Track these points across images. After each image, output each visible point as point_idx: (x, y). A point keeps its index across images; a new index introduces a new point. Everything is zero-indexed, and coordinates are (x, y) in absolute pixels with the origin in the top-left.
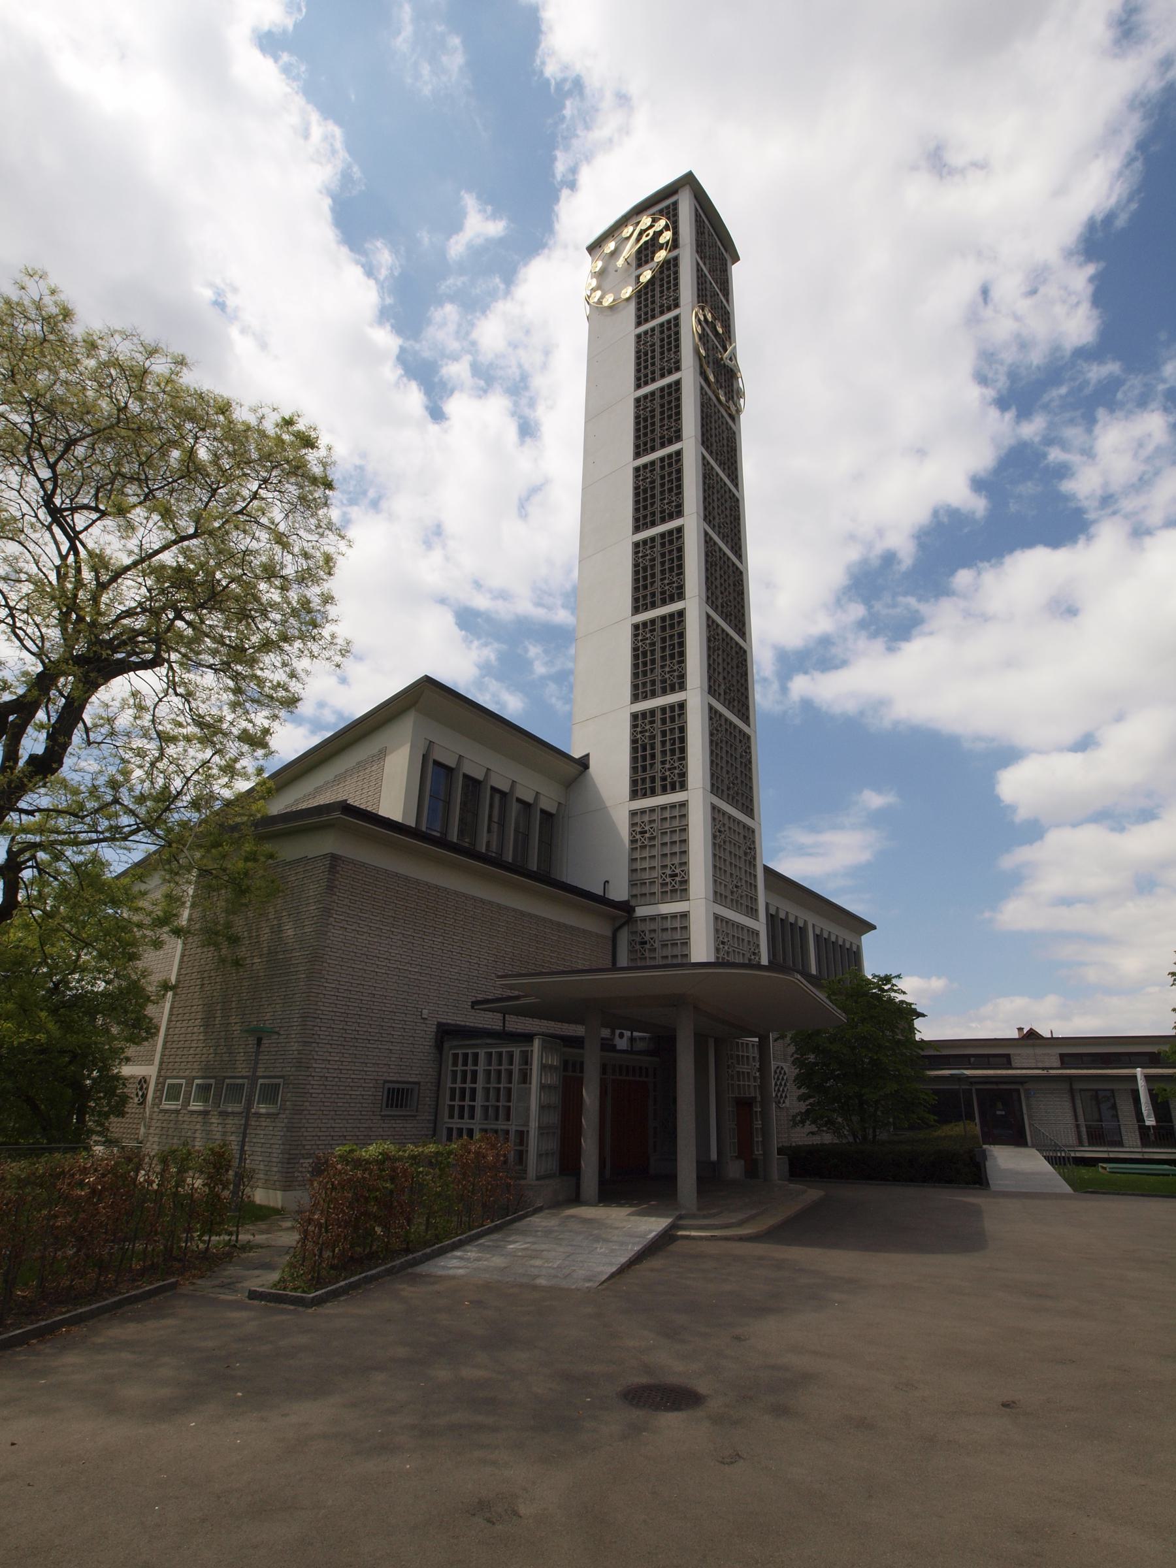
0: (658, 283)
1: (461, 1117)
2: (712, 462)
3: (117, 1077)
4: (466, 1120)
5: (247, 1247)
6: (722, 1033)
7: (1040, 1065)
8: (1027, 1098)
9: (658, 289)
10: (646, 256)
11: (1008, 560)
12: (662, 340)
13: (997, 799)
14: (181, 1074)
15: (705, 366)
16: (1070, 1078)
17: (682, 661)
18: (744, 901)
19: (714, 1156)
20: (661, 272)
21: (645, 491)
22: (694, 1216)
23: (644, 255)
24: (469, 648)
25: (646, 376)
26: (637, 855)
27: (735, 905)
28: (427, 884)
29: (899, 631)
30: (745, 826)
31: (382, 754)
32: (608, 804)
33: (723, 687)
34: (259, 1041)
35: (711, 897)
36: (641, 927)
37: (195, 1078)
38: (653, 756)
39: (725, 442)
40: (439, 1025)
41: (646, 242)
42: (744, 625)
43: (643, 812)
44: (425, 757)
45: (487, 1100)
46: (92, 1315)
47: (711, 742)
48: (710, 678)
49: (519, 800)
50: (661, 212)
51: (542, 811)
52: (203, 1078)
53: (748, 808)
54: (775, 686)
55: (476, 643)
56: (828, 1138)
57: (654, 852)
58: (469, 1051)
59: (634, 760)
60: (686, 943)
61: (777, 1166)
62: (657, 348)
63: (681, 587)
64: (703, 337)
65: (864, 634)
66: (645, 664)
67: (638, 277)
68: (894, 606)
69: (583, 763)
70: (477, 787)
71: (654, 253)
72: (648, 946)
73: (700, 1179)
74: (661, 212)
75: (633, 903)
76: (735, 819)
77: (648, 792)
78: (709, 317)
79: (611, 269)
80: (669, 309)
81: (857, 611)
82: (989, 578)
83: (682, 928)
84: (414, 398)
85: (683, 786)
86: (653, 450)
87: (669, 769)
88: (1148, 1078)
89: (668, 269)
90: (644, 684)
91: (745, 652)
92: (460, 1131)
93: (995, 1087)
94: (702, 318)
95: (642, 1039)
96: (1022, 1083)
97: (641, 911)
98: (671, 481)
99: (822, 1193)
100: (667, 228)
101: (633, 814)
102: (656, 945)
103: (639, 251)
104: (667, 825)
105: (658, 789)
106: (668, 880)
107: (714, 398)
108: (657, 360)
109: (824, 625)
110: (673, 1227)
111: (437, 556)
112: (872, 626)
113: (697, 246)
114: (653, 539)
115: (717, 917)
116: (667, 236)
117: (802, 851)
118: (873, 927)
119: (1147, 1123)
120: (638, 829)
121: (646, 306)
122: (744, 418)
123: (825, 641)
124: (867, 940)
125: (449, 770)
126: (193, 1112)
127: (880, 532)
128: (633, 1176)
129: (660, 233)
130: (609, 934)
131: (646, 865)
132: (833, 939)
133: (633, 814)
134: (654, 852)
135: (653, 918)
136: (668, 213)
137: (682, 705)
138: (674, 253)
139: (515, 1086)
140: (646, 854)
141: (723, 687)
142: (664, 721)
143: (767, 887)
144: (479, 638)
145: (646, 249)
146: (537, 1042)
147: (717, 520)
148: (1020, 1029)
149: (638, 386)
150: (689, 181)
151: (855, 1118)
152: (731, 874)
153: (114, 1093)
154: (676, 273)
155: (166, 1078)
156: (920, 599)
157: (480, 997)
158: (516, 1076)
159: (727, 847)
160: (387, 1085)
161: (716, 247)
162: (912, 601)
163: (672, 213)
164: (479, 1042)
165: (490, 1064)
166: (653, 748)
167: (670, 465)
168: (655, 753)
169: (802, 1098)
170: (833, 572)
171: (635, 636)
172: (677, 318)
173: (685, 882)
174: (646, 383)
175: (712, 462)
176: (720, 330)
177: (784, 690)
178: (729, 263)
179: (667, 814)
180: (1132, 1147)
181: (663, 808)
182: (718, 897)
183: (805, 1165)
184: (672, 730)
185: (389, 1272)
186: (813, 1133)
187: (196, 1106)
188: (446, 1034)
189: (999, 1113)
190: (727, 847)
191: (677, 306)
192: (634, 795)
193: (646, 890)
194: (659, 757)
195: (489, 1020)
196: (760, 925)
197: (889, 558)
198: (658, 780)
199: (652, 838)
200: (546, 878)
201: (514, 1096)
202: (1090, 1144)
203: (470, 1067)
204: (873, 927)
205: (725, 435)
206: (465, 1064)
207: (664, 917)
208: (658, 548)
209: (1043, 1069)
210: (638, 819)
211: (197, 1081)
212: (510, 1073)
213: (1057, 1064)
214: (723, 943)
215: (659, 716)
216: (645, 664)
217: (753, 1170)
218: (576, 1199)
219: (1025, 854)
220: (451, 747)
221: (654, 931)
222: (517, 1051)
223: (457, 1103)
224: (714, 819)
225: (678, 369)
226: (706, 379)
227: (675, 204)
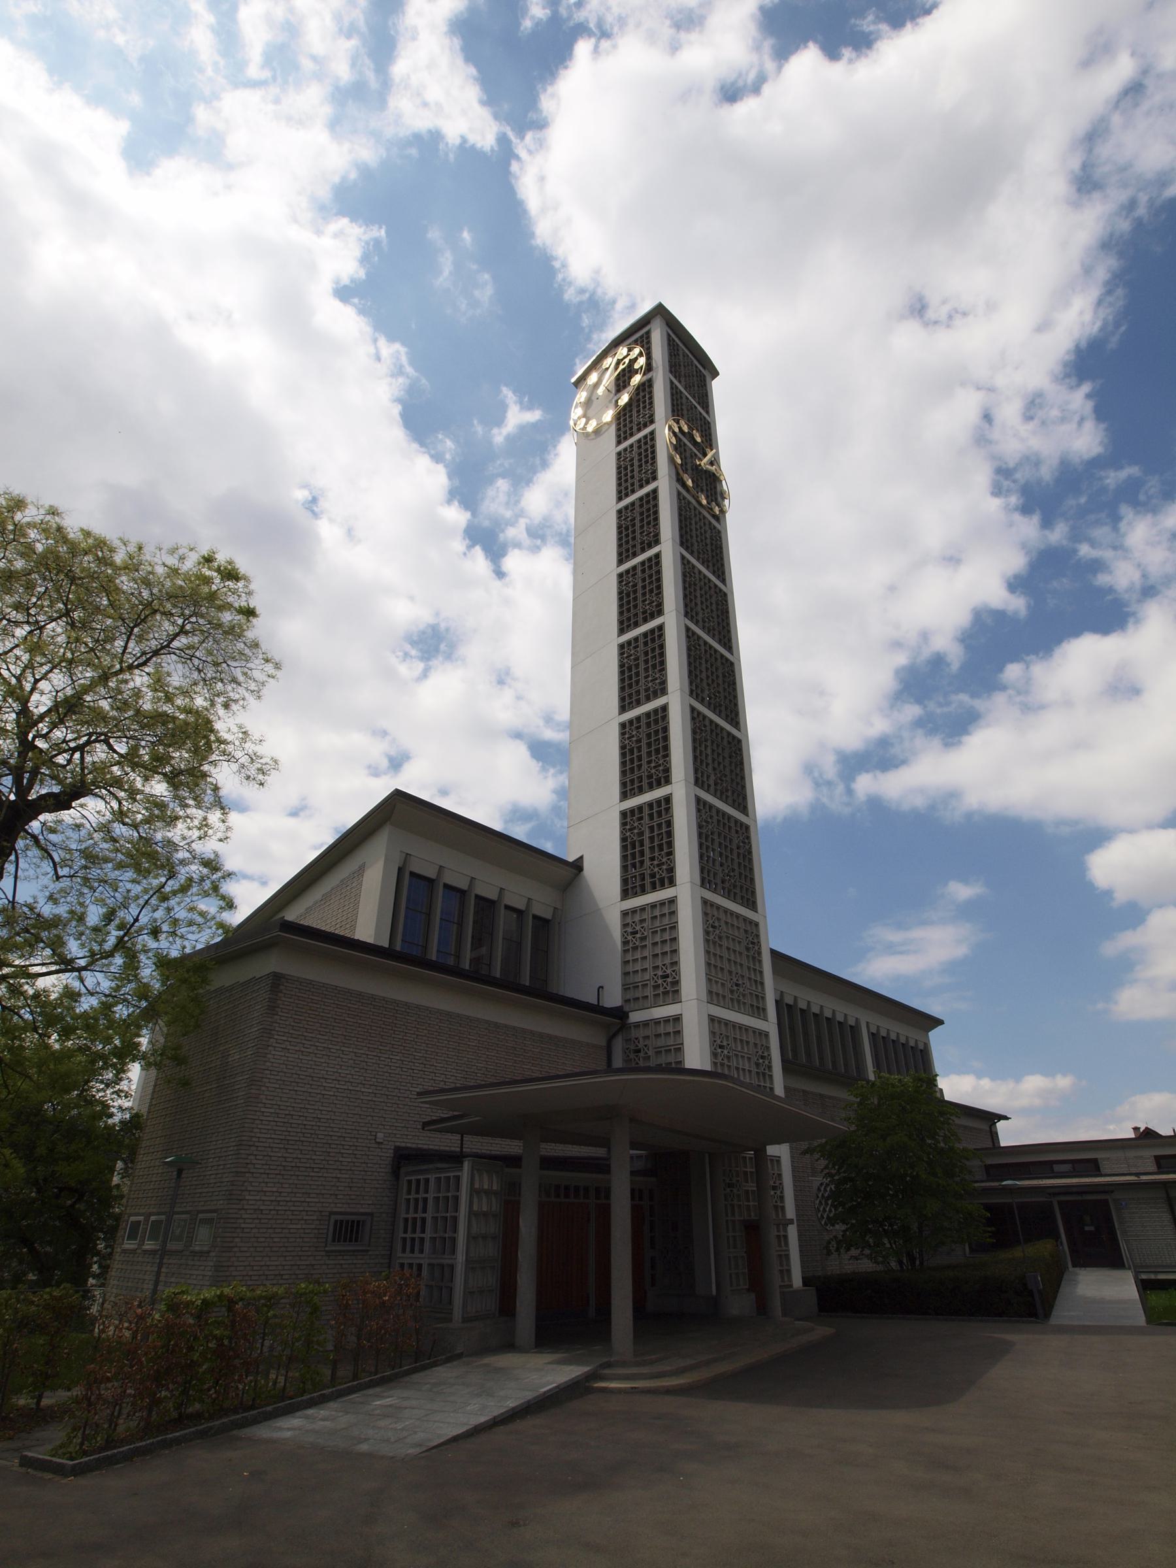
0: (635, 404)
2: (694, 561)
4: (417, 1254)
7: (1134, 1170)
11: (1058, 652)
12: (640, 454)
15: (681, 472)
17: (667, 755)
18: (748, 1000)
20: (638, 394)
22: (624, 1364)
23: (621, 382)
24: (546, 778)
25: (626, 488)
27: (736, 1003)
28: (384, 999)
29: (955, 728)
30: (745, 919)
31: (361, 869)
33: (713, 777)
34: (180, 1172)
36: (634, 1033)
37: (151, 1214)
38: (642, 853)
41: (623, 370)
43: (634, 911)
47: (700, 835)
48: (696, 771)
50: (636, 342)
51: (535, 917)
55: (552, 771)
57: (646, 953)
60: (679, 1049)
62: (636, 463)
63: (664, 683)
64: (679, 447)
65: (920, 732)
67: (617, 402)
68: (948, 704)
69: (577, 866)
72: (642, 1054)
75: (626, 1009)
76: (732, 913)
78: (686, 429)
79: (594, 398)
80: (645, 426)
81: (912, 711)
82: (1038, 669)
85: (672, 882)
86: (635, 555)
89: (644, 390)
90: (632, 781)
93: (1079, 1198)
94: (677, 430)
97: (635, 1017)
99: (829, 1331)
100: (641, 354)
101: (625, 914)
102: (650, 1053)
103: (618, 378)
104: (657, 923)
105: (648, 887)
106: (660, 981)
107: (693, 501)
109: (880, 726)
111: (508, 695)
112: (928, 725)
113: (671, 367)
115: (712, 1019)
116: (642, 361)
118: (941, 1022)
120: (629, 930)
122: (730, 518)
123: (883, 742)
124: (935, 1036)
126: (145, 1252)
127: (925, 636)
128: (570, 1319)
129: (636, 359)
130: (604, 1043)
131: (638, 967)
132: (903, 1040)
133: (625, 914)
134: (646, 953)
135: (646, 1024)
137: (668, 799)
140: (638, 955)
141: (713, 777)
142: (651, 816)
144: (554, 766)
145: (624, 375)
146: (466, 1165)
147: (701, 615)
148: (1136, 1129)
149: (620, 499)
150: (660, 311)
154: (651, 393)
156: (974, 695)
157: (428, 1119)
159: (725, 943)
161: (691, 368)
162: (964, 697)
163: (645, 342)
164: (431, 1166)
166: (642, 845)
168: (644, 848)
170: (882, 676)
172: (652, 433)
173: (677, 983)
174: (627, 495)
175: (694, 561)
176: (699, 440)
177: (850, 792)
178: (708, 378)
179: (657, 912)
181: (653, 906)
182: (713, 996)
184: (660, 825)
185: (203, 1434)
187: (149, 1245)
188: (404, 1158)
189: (1087, 1228)
191: (652, 422)
192: (626, 894)
193: (639, 994)
194: (647, 854)
195: (448, 1142)
196: (770, 1025)
198: (647, 877)
199: (643, 939)
203: (422, 1195)
204: (941, 1022)
207: (657, 1022)
208: (641, 647)
209: (1137, 1175)
210: (629, 920)
211: (153, 1218)
213: (1154, 1168)
214: (721, 1047)
215: (646, 811)
218: (509, 1346)
220: (430, 859)
221: (648, 1037)
224: (705, 914)
226: (684, 485)
227: (648, 333)
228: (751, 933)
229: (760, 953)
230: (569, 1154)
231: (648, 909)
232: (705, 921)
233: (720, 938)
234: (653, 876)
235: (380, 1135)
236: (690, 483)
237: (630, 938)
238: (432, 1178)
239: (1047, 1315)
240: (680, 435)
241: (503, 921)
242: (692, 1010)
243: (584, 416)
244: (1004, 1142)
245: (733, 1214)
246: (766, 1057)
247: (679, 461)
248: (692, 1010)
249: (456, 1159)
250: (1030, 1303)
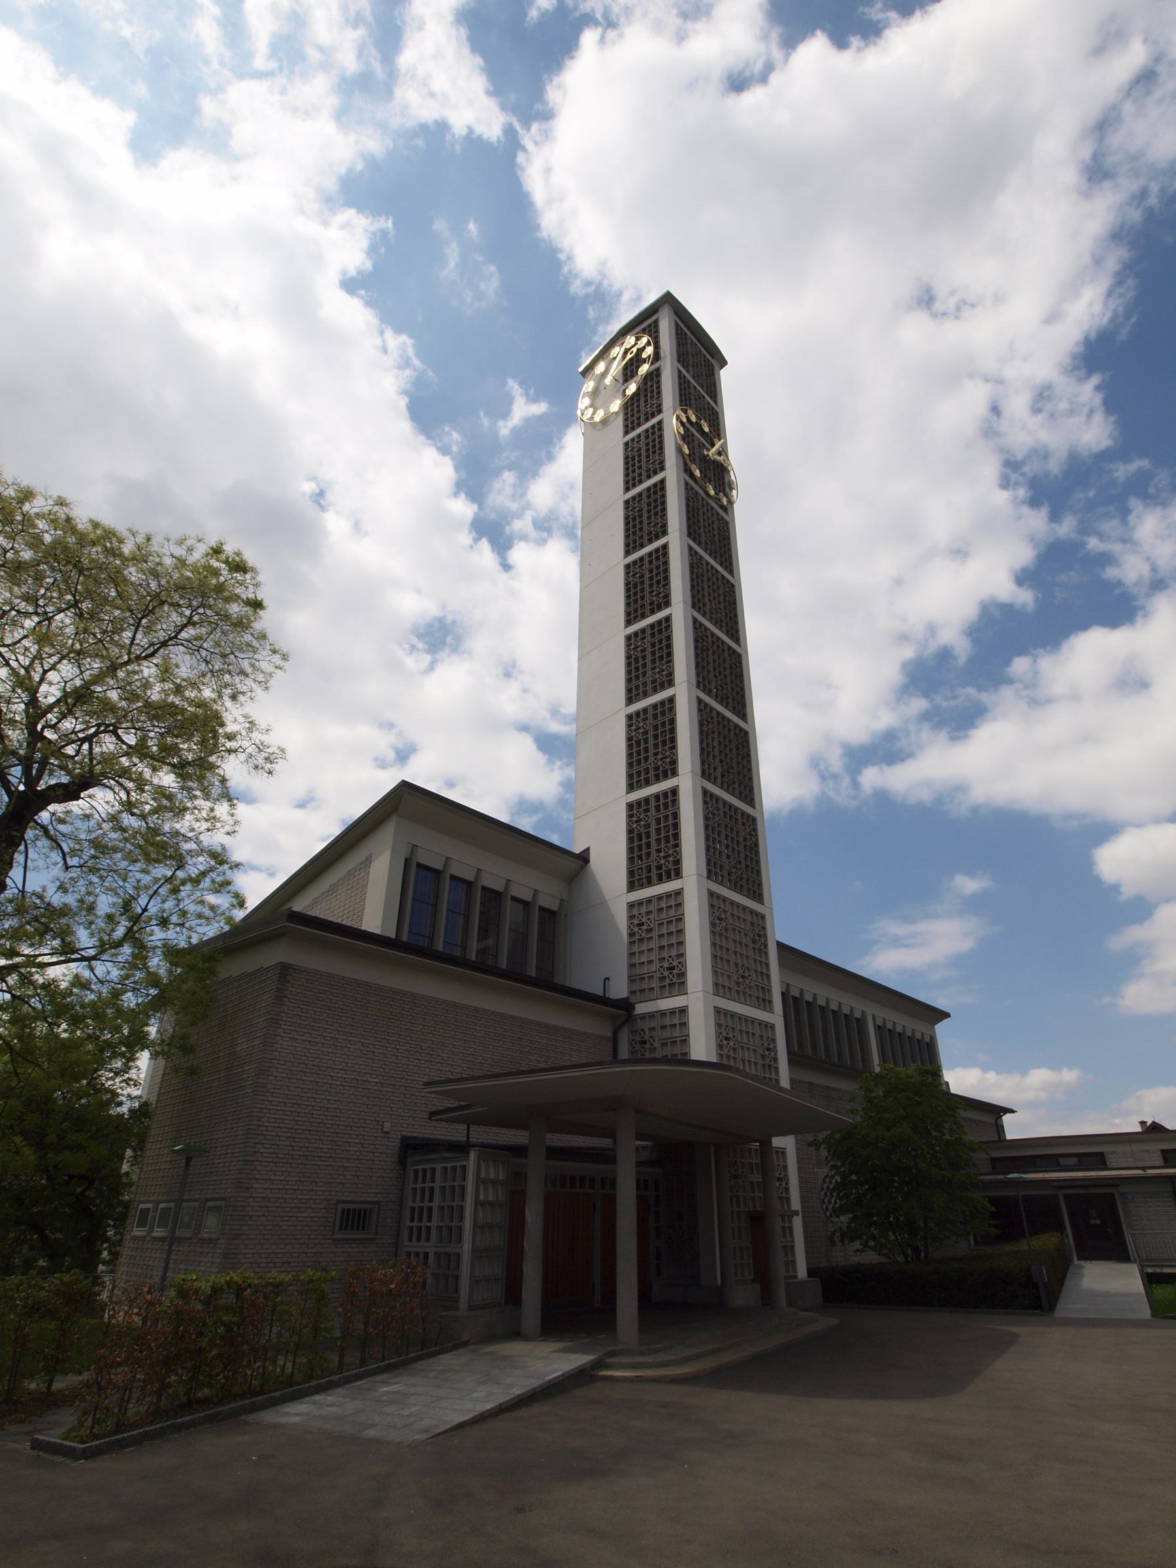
0: (642, 394)
2: (701, 552)
9: (642, 400)
10: (632, 371)
12: (647, 444)
13: (1098, 880)
17: (674, 747)
20: (645, 384)
21: (635, 586)
23: (629, 371)
24: (552, 770)
25: (634, 479)
26: (636, 949)
27: (742, 996)
29: (961, 722)
30: (752, 912)
31: (368, 862)
33: (719, 770)
34: (189, 1160)
35: (710, 989)
36: (640, 1025)
38: (648, 845)
41: (631, 359)
42: (744, 706)
43: (640, 903)
46: (186, 1426)
47: (707, 827)
48: (703, 762)
49: (515, 899)
50: (644, 331)
52: (167, 1201)
53: (756, 891)
54: (846, 782)
55: (558, 763)
59: (630, 850)
60: (685, 1041)
64: (687, 437)
65: (926, 726)
66: (639, 753)
67: (624, 391)
68: (955, 697)
69: (584, 858)
70: (448, 889)
72: (647, 1046)
75: (632, 1000)
77: (645, 881)
78: (693, 419)
79: (601, 387)
81: (919, 704)
83: (681, 1024)
84: (486, 555)
85: (678, 874)
87: (664, 857)
89: (652, 380)
94: (684, 420)
97: (641, 1009)
100: (648, 344)
101: (631, 906)
102: (656, 1045)
103: (625, 368)
106: (666, 973)
107: (701, 492)
108: (643, 463)
109: (886, 719)
110: (599, 1364)
111: (514, 688)
114: (643, 631)
115: (718, 1011)
116: (650, 350)
117: (896, 942)
118: (947, 1015)
120: (636, 922)
121: (633, 415)
122: (738, 509)
123: (890, 736)
124: (941, 1030)
127: (932, 629)
128: (574, 1308)
129: (644, 348)
130: (609, 1034)
131: (644, 959)
133: (631, 906)
134: (652, 945)
135: (652, 1015)
137: (674, 791)
140: (644, 947)
141: (719, 770)
142: (658, 808)
145: (632, 365)
150: (668, 300)
152: (736, 964)
156: (980, 689)
157: (435, 1109)
159: (731, 934)
160: (341, 1206)
161: (699, 357)
162: (971, 691)
163: (653, 332)
164: (437, 1156)
166: (648, 836)
168: (651, 841)
170: (888, 669)
171: (629, 726)
173: (683, 975)
174: (634, 486)
175: (701, 552)
176: (707, 429)
177: (856, 785)
179: (663, 905)
181: (660, 898)
182: (719, 988)
184: (666, 817)
185: (211, 1419)
187: (158, 1232)
190: (731, 934)
192: (632, 886)
193: (645, 985)
196: (776, 1018)
197: (945, 654)
198: (653, 869)
199: (650, 930)
200: (548, 983)
204: (947, 1015)
205: (716, 526)
207: (663, 1014)
211: (162, 1205)
214: (727, 1039)
215: (653, 803)
216: (639, 753)
219: (1135, 934)
220: (436, 850)
221: (654, 1029)
223: (415, 1224)
224: (712, 906)
226: (692, 475)
227: (656, 321)
228: (758, 925)
229: (766, 946)
230: (574, 1144)
231: (655, 901)
233: (726, 930)
235: (387, 1125)
236: (697, 473)
237: (636, 929)
238: (439, 1167)
239: (1052, 1308)
245: (738, 1206)
246: (771, 1048)
247: (687, 451)
249: (462, 1148)
250: (1034, 1295)
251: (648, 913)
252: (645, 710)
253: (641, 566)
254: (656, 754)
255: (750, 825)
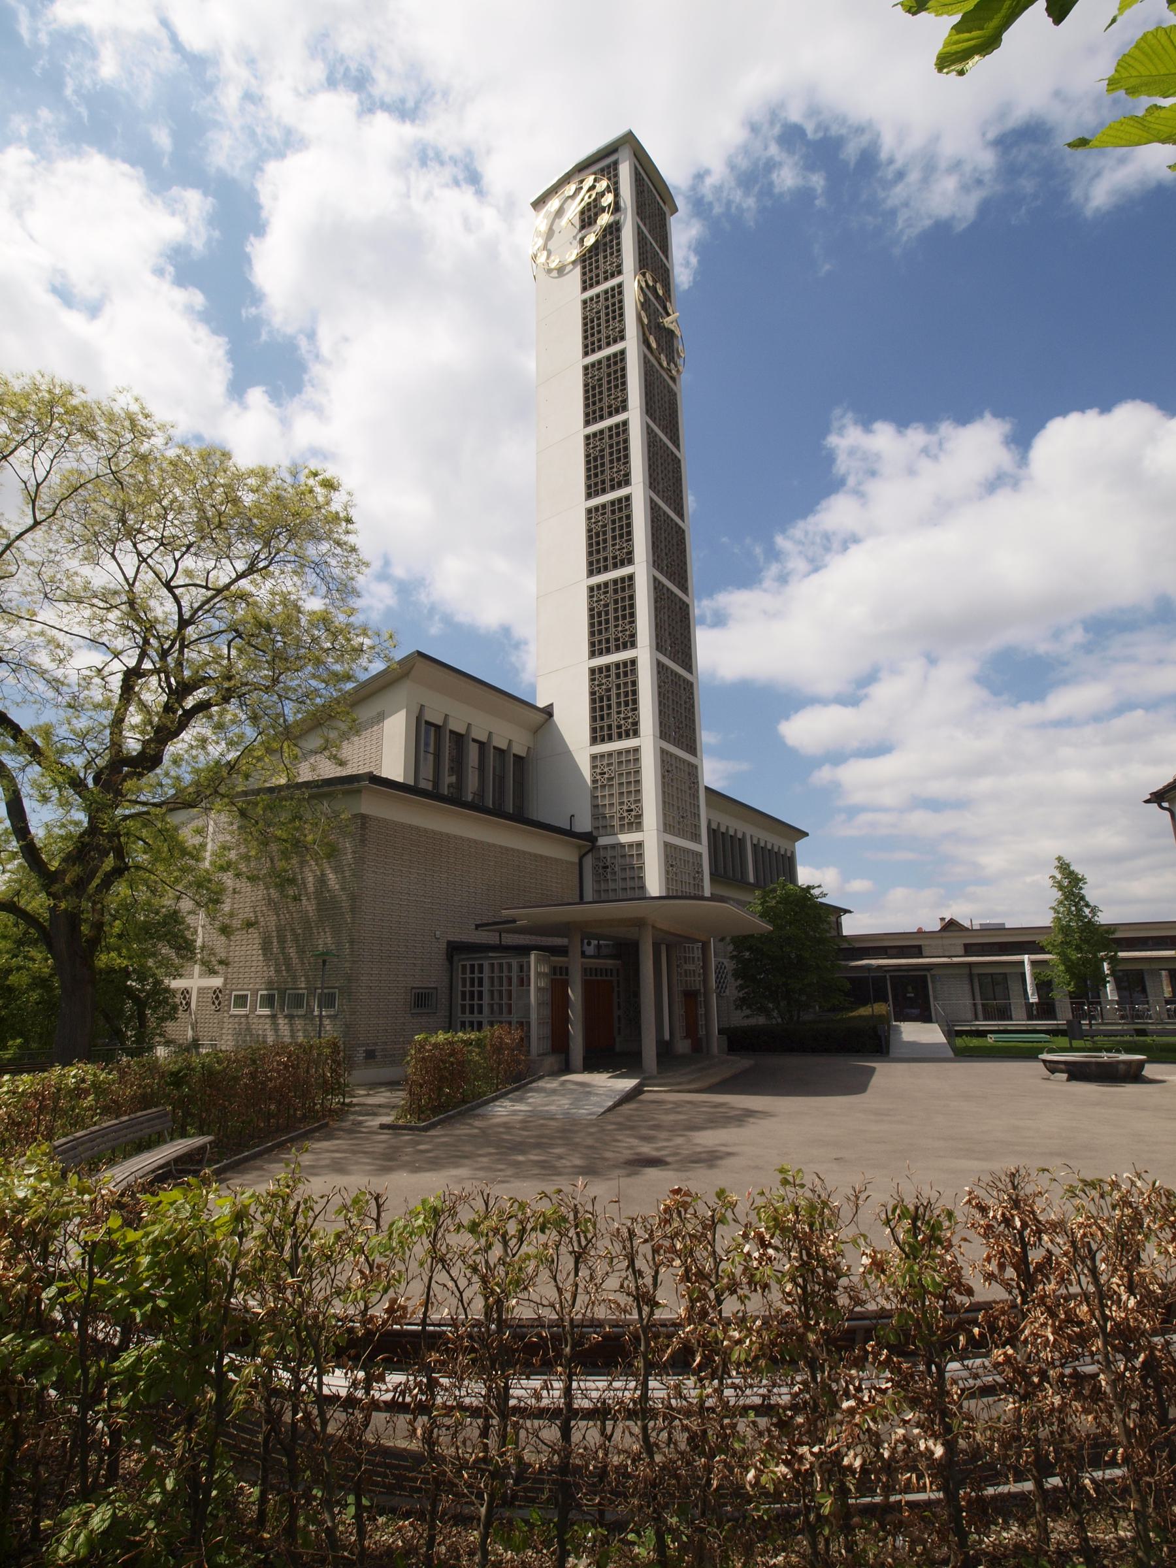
0: (601, 248)
1: (472, 1012)
3: (167, 990)
5: (350, 1105)
6: (672, 945)
8: (933, 982)
14: (245, 987)
15: (647, 333)
16: (970, 964)
19: (667, 1037)
20: (604, 236)
22: (654, 1078)
23: (588, 218)
27: (681, 834)
31: (381, 717)
32: (571, 748)
33: (669, 642)
37: (258, 990)
39: (667, 406)
40: (449, 943)
41: (589, 204)
43: (602, 756)
44: (418, 719)
45: (492, 999)
47: (659, 693)
53: (692, 748)
56: (761, 1020)
58: (476, 963)
61: (716, 1043)
63: (627, 475)
64: (645, 305)
67: (582, 240)
69: (548, 712)
71: (596, 215)
73: (658, 1055)
74: (602, 170)
85: (636, 733)
88: (1034, 963)
91: (688, 606)
92: (472, 1023)
94: (644, 285)
95: (608, 945)
96: (928, 970)
97: (603, 841)
98: (616, 379)
99: (752, 1062)
100: (608, 189)
101: (594, 758)
105: (615, 736)
106: (625, 814)
107: (656, 363)
115: (666, 844)
116: (609, 199)
118: (806, 834)
119: (1031, 1001)
120: (598, 771)
124: (800, 846)
125: (437, 727)
128: (604, 1055)
129: (602, 194)
130: (576, 860)
133: (594, 758)
135: (613, 847)
136: (609, 173)
138: (617, 216)
139: (514, 988)
142: (618, 676)
143: (708, 804)
145: (589, 210)
149: (584, 289)
150: (629, 141)
151: (783, 1003)
153: (166, 1004)
155: (233, 990)
158: (515, 980)
163: (611, 171)
165: (493, 972)
166: (609, 699)
167: (618, 434)
168: (611, 703)
169: (741, 988)
173: (639, 816)
176: (660, 292)
180: (1019, 1021)
181: (620, 753)
183: (739, 1041)
184: (626, 684)
186: (747, 1017)
188: (455, 949)
190: (674, 784)
191: (620, 272)
192: (594, 741)
196: (703, 848)
201: (514, 995)
202: (985, 1019)
204: (806, 834)
205: (667, 399)
206: (472, 972)
211: (260, 993)
212: (510, 979)
213: (962, 953)
215: (613, 671)
217: (699, 1047)
218: (567, 1069)
222: (515, 963)
225: (623, 338)
226: (649, 346)
227: (616, 163)
228: (693, 772)
231: (615, 756)
232: (663, 766)
234: (619, 727)
236: (654, 345)
237: (598, 777)
238: (486, 964)
240: (646, 290)
241: (473, 752)
242: (649, 837)
243: (545, 247)
244: (846, 932)
246: (700, 872)
247: (646, 321)
248: (649, 837)
249: (525, 950)
250: (877, 1044)
251: (609, 765)
252: (606, 584)
253: (601, 439)
254: (616, 626)
255: (689, 687)
